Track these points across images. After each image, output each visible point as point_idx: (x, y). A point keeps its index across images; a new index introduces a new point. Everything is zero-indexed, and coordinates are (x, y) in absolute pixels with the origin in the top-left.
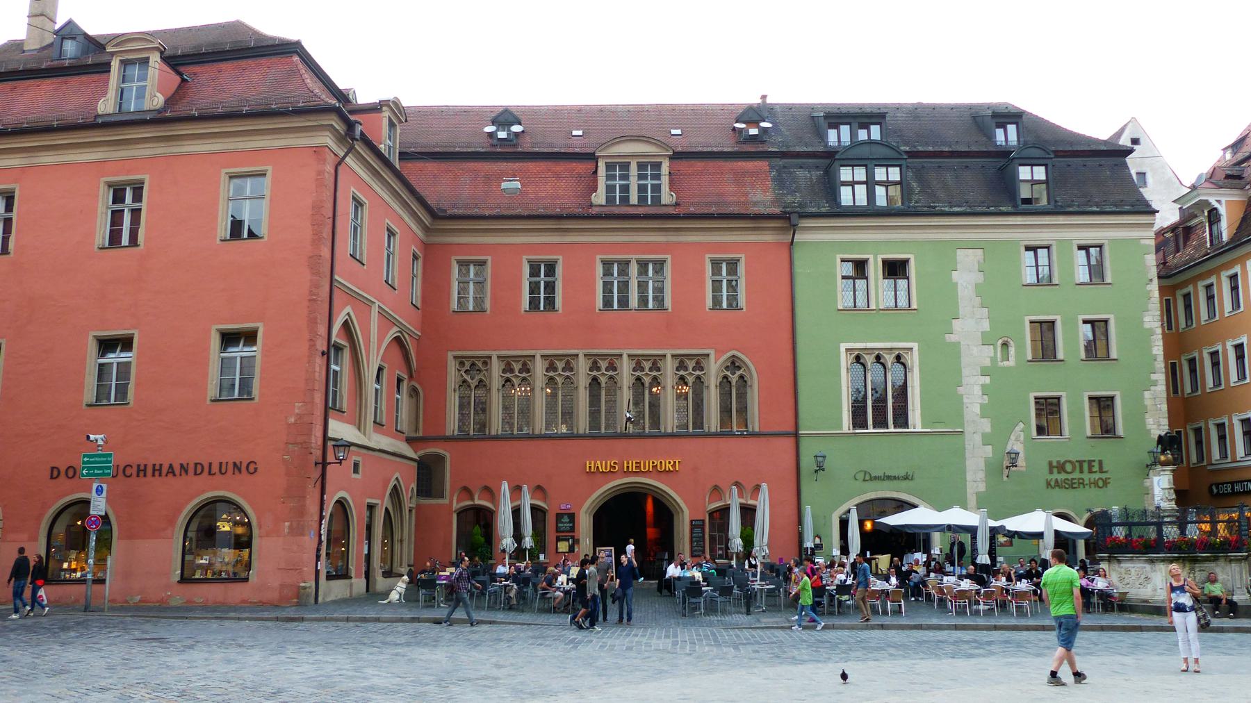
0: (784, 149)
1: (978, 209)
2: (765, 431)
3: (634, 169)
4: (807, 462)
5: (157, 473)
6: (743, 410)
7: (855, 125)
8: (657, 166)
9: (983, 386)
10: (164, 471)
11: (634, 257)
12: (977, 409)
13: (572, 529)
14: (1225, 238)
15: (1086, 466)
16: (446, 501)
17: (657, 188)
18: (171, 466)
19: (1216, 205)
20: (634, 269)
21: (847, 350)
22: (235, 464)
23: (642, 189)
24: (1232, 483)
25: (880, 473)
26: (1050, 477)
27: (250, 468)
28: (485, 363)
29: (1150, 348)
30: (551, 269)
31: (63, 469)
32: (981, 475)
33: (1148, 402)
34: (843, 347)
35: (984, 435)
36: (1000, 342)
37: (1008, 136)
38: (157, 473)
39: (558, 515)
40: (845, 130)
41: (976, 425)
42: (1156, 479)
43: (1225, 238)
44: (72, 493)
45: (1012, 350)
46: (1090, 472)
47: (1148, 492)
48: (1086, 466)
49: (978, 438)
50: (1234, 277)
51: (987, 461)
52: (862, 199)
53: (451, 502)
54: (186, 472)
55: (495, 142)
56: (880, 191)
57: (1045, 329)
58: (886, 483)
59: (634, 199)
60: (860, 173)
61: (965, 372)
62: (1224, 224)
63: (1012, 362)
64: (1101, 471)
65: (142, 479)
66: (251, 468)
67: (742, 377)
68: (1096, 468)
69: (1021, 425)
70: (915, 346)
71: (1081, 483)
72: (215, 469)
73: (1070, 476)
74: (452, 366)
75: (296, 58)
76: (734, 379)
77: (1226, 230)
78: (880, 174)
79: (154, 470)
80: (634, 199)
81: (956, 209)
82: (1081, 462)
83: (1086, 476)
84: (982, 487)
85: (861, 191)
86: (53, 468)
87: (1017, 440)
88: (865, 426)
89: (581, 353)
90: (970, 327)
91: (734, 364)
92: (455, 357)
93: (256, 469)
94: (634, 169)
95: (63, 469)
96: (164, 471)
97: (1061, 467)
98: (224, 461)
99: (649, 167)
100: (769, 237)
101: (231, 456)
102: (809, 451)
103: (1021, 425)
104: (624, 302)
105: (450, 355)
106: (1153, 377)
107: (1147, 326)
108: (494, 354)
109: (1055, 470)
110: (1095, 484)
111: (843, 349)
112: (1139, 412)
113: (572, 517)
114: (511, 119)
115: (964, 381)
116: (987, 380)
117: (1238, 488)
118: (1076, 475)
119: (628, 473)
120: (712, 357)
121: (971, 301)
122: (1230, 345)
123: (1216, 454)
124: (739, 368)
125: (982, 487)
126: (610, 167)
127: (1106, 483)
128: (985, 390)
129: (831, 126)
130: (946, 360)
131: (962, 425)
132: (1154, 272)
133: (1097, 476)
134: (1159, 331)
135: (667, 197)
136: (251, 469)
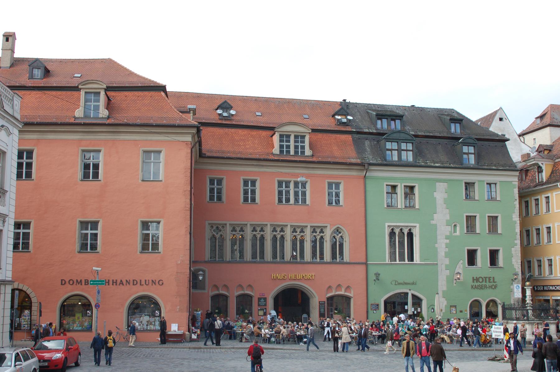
0: (358, 130)
1: (446, 165)
2: (352, 261)
3: (292, 139)
4: (372, 277)
5: (115, 284)
6: (341, 253)
7: (389, 119)
8: (303, 137)
9: (446, 244)
10: (118, 282)
11: (293, 180)
12: (443, 254)
13: (265, 305)
14: (544, 181)
15: (487, 279)
16: (206, 291)
17: (303, 147)
18: (121, 281)
19: (541, 165)
20: (292, 185)
21: (388, 226)
22: (152, 281)
23: (296, 147)
24: (543, 286)
25: (402, 282)
26: (473, 284)
27: (160, 283)
28: (223, 227)
29: (515, 229)
30: (254, 183)
31: (67, 281)
32: (445, 283)
33: (513, 253)
34: (387, 224)
35: (446, 265)
36: (453, 225)
37: (455, 129)
38: (115, 284)
39: (258, 298)
40: (385, 121)
41: (443, 260)
42: (515, 285)
43: (544, 181)
44: (72, 291)
45: (458, 228)
46: (489, 282)
47: (512, 291)
48: (487, 279)
49: (444, 267)
50: (547, 198)
51: (447, 276)
52: (395, 158)
53: (208, 292)
54: (129, 284)
55: (222, 118)
56: (404, 153)
57: (471, 220)
58: (405, 286)
59: (292, 153)
60: (395, 146)
61: (439, 237)
62: (544, 174)
63: (458, 233)
64: (494, 282)
65: (107, 286)
66: (161, 283)
67: (341, 237)
68: (492, 280)
69: (462, 261)
70: (418, 225)
71: (486, 287)
72: (143, 283)
73: (481, 284)
74: (208, 228)
75: (163, 94)
76: (338, 238)
77: (544, 176)
78: (403, 146)
79: (113, 282)
80: (292, 153)
81: (437, 165)
82: (486, 278)
83: (488, 284)
84: (445, 288)
85: (395, 153)
86: (62, 280)
87: (459, 268)
88: (395, 261)
89: (269, 224)
90: (441, 217)
91: (338, 230)
92: (209, 224)
93: (163, 283)
94: (292, 139)
95: (67, 281)
96: (118, 282)
97: (477, 280)
98: (147, 279)
99: (299, 138)
100: (354, 173)
101: (150, 277)
102: (372, 270)
103: (462, 261)
104: (288, 200)
105: (207, 223)
106: (516, 242)
107: (514, 220)
108: (228, 223)
109: (475, 281)
110: (491, 287)
111: (386, 226)
112: (509, 257)
113: (265, 299)
114: (228, 106)
115: (438, 241)
116: (448, 241)
117: (545, 288)
118: (484, 283)
119: (291, 279)
120: (329, 227)
121: (441, 205)
122: (544, 227)
123: (537, 273)
124: (340, 233)
125: (445, 288)
126: (281, 136)
127: (496, 287)
128: (447, 246)
129: (379, 119)
130: (431, 232)
131: (437, 261)
132: (517, 196)
133: (492, 284)
134: (518, 222)
135: (308, 152)
136: (161, 283)
